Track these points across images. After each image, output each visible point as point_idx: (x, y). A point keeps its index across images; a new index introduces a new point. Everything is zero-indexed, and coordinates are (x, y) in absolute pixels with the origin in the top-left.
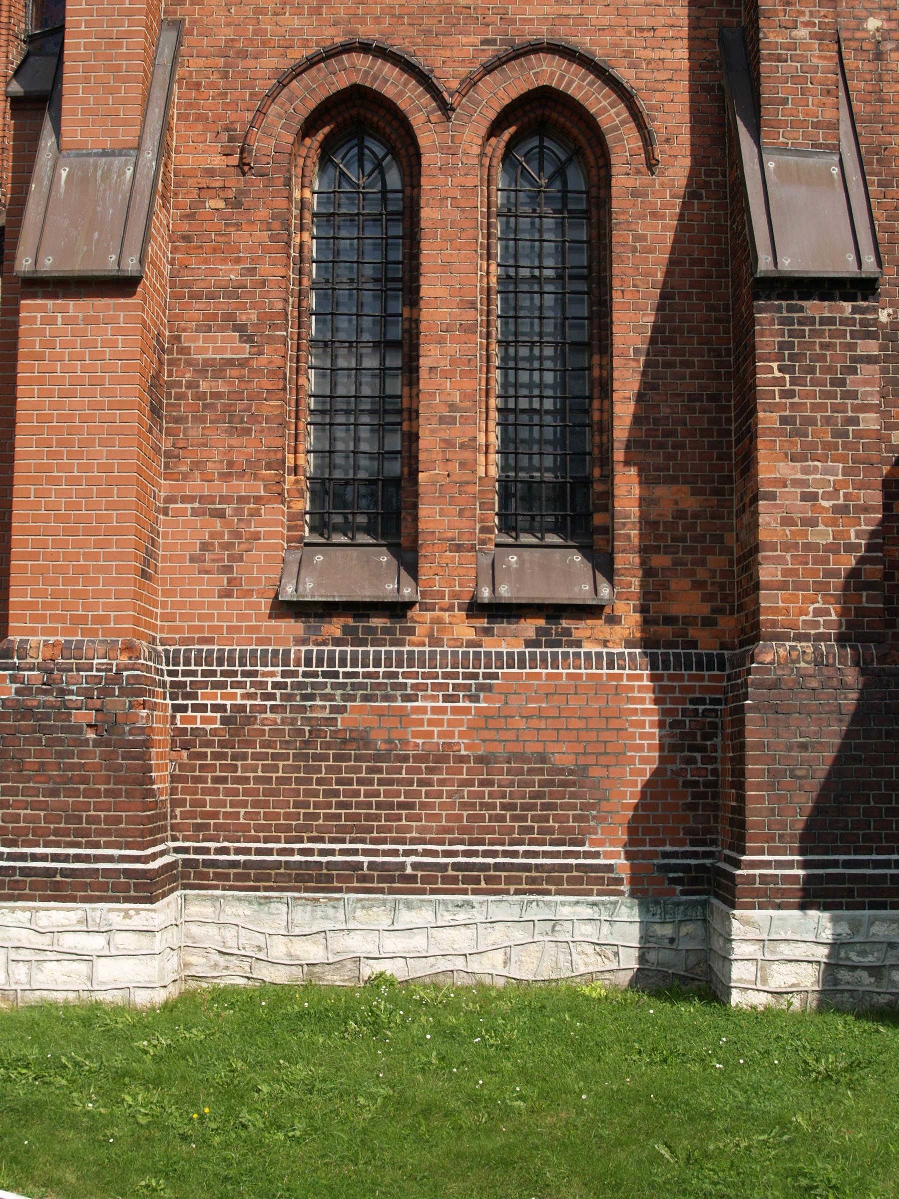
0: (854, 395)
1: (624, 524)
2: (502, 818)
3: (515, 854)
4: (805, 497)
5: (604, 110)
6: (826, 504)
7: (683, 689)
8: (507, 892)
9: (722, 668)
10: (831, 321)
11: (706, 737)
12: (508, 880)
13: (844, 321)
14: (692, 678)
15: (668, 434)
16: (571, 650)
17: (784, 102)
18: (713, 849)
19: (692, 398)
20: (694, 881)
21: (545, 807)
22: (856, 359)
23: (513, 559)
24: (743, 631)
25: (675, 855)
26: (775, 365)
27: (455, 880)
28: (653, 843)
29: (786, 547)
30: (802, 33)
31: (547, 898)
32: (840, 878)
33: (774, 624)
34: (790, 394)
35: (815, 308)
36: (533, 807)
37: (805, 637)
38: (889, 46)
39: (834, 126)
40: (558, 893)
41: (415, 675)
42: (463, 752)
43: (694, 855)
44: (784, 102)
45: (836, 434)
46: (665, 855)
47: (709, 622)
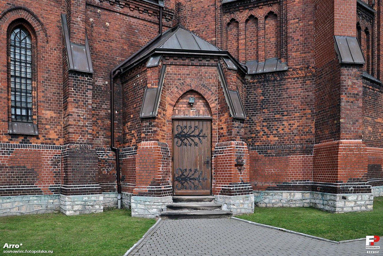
0: (87, 96)
1: (40, 119)
2: (16, 180)
3: (19, 187)
4: (78, 116)
5: (36, 27)
6: (82, 117)
7: (53, 153)
8: (18, 195)
9: (60, 149)
10: (83, 81)
11: (58, 163)
12: (18, 193)
13: (86, 81)
14: (54, 151)
15: (49, 100)
16: (30, 144)
17: (75, 33)
18: (60, 185)
19: (54, 93)
20: (56, 191)
21: (25, 177)
22: (88, 89)
23: (16, 124)
24: (65, 142)
25: (52, 186)
26: (72, 88)
27: (6, 193)
28: (48, 184)
29: (75, 125)
30: (79, 19)
31: (27, 196)
32: (86, 189)
33: (72, 140)
34: (75, 95)
35: (80, 77)
36: (23, 177)
37: (78, 143)
38: (94, 25)
39: (85, 40)
40: (29, 195)
41: (99, 152)
42: (7, 166)
43: (56, 186)
44: (75, 33)
45: (84, 104)
46: (50, 186)
47: (58, 140)
